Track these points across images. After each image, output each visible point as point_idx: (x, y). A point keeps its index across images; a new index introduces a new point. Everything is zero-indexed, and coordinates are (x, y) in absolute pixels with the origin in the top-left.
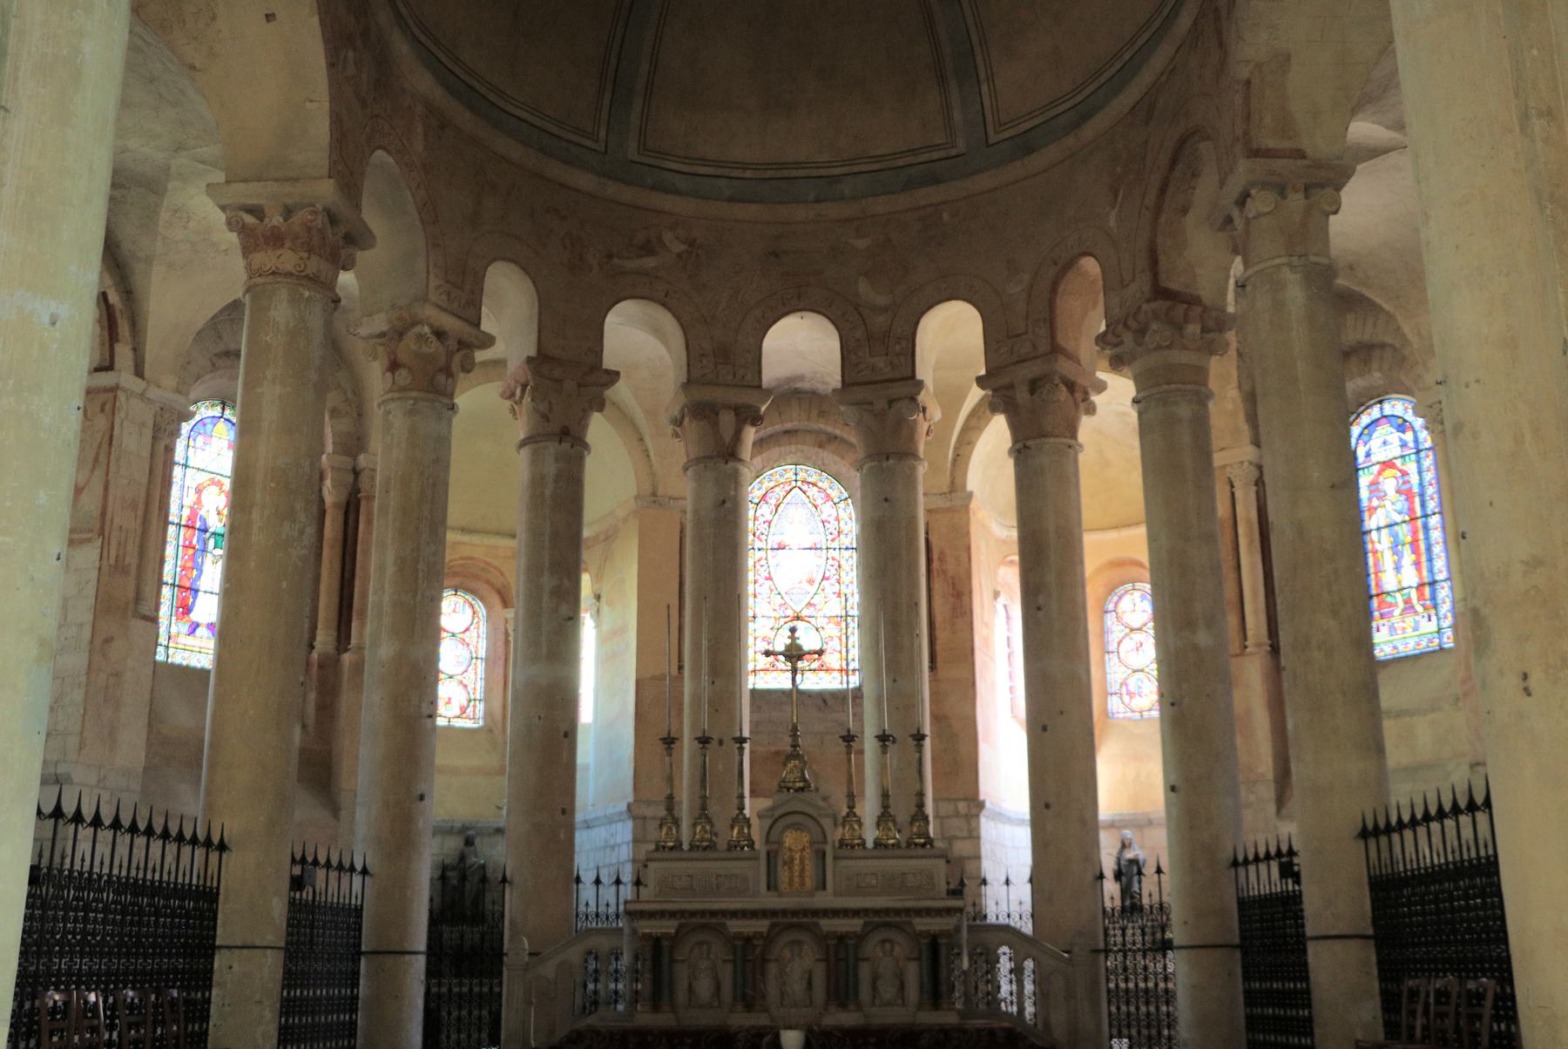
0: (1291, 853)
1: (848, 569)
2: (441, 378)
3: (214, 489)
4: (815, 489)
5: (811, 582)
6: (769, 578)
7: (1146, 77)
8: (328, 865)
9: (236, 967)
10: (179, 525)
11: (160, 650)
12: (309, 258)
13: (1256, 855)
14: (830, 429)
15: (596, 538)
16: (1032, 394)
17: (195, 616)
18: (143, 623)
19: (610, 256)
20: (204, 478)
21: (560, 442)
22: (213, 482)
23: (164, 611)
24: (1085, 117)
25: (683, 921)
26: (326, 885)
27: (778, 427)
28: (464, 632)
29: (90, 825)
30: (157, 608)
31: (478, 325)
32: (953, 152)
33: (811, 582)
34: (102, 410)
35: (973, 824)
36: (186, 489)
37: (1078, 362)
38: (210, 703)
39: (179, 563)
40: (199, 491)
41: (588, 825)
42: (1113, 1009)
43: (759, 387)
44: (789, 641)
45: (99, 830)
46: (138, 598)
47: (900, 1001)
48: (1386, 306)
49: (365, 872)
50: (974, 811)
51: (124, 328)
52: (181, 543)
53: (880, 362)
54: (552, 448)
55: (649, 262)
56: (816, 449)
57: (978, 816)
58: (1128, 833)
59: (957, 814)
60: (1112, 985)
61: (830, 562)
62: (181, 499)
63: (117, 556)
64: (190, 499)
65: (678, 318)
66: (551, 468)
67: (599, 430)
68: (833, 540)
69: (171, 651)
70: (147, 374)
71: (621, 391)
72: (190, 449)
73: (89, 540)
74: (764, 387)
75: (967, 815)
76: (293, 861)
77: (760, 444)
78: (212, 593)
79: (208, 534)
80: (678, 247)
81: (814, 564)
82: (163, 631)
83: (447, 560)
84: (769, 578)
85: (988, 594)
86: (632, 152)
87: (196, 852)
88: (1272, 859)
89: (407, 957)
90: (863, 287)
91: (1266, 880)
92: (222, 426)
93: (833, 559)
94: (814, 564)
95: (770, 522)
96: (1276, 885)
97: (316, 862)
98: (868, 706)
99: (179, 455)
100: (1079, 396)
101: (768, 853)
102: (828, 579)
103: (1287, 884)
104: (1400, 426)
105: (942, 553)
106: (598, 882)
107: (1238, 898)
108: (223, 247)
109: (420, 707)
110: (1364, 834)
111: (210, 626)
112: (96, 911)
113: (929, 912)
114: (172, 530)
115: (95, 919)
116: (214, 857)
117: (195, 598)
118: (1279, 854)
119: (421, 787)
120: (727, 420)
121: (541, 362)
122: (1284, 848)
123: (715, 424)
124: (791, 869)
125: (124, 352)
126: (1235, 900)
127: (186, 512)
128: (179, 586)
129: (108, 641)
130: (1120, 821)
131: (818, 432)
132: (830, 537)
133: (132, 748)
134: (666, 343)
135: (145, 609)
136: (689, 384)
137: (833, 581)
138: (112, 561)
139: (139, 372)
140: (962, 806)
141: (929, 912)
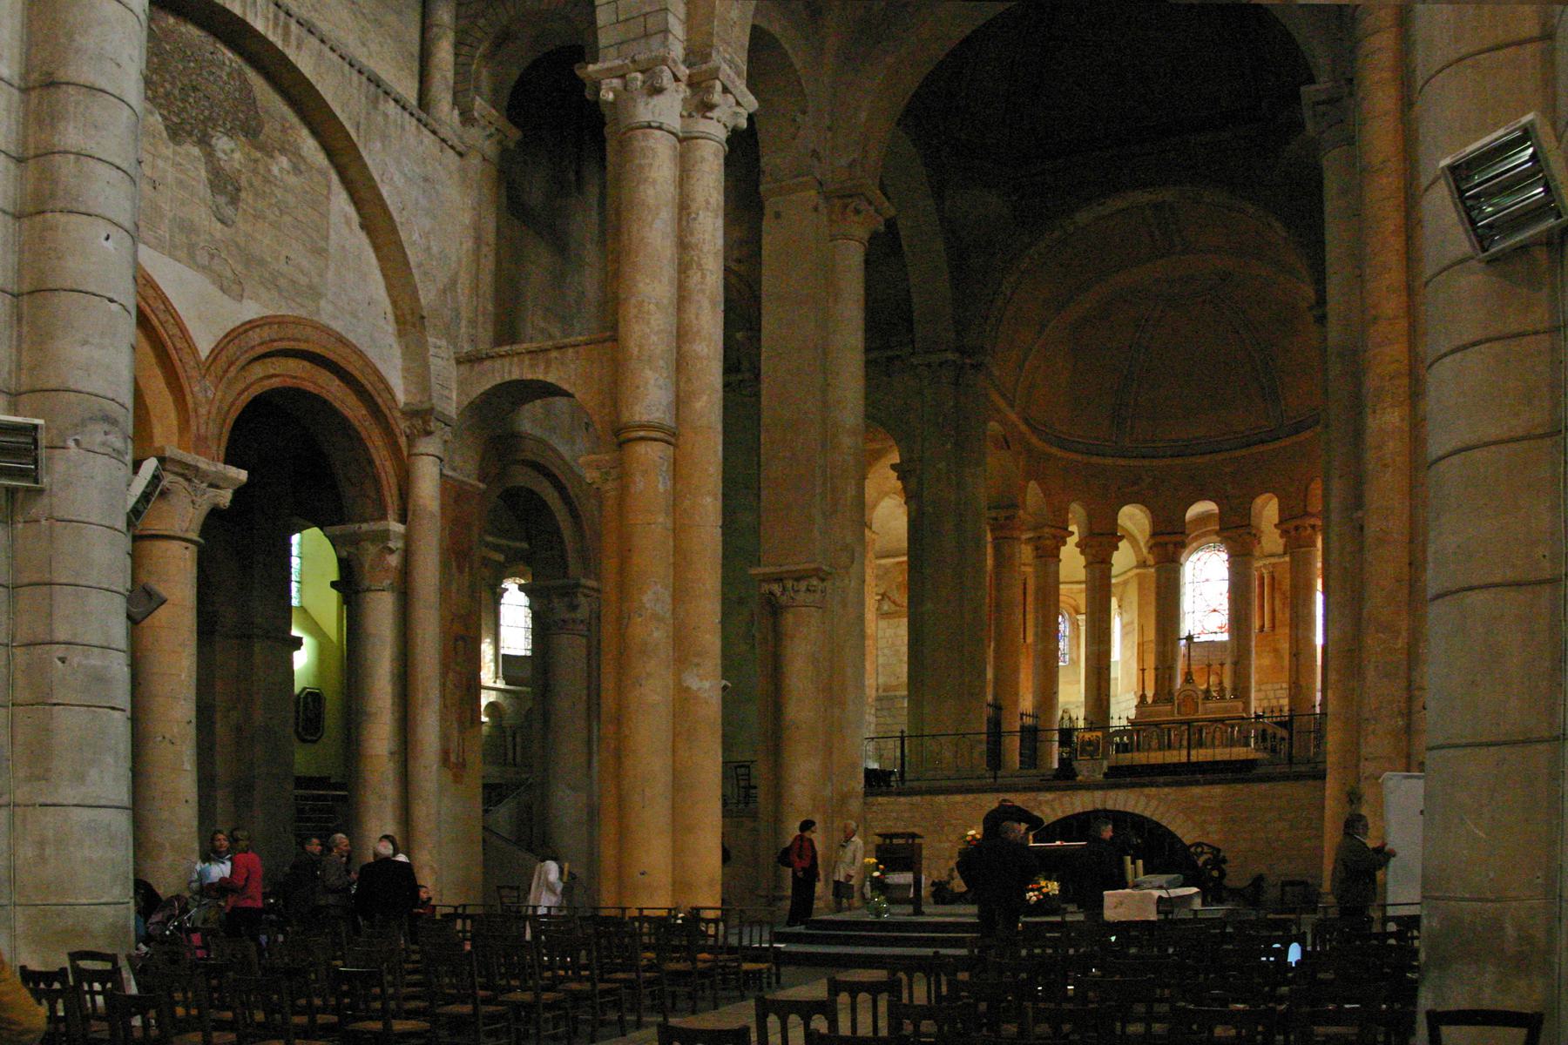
2: (1055, 551)
120: (1171, 547)
136: (1154, 534)
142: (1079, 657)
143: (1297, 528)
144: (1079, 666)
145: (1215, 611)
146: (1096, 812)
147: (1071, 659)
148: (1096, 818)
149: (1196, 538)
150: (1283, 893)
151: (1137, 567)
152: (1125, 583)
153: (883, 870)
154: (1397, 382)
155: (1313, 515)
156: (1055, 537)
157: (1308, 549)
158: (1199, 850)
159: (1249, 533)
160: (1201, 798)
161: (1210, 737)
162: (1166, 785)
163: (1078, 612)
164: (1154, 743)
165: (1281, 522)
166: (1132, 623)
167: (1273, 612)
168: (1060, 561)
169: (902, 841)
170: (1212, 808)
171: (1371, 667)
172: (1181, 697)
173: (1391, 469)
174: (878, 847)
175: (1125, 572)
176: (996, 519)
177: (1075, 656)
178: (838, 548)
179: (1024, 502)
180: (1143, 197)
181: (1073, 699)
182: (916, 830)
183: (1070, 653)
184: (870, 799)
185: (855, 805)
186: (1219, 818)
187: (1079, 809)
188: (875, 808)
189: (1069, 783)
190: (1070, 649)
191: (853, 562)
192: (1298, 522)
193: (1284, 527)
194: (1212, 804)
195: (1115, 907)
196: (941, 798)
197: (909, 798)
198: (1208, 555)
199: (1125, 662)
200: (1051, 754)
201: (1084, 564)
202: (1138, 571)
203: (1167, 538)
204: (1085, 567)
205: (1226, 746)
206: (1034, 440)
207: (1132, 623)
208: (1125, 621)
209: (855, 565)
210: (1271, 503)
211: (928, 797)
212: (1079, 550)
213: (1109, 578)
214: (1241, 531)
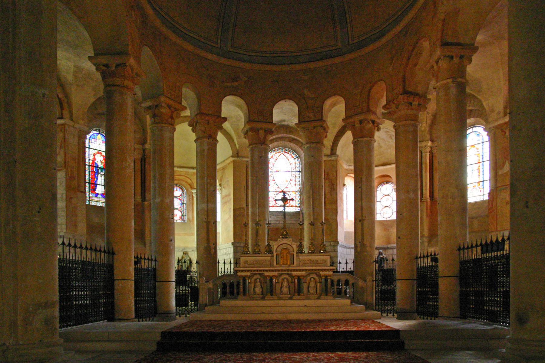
0: (435, 255)
1: (298, 178)
3: (99, 155)
4: (288, 154)
5: (287, 181)
6: (274, 180)
7: (405, 21)
8: (145, 259)
9: (121, 285)
10: (89, 165)
11: (87, 201)
12: (125, 81)
13: (464, 247)
14: (293, 136)
15: (220, 169)
16: (360, 124)
17: (97, 191)
18: (81, 194)
20: (95, 152)
21: (209, 139)
22: (98, 153)
23: (87, 190)
24: (383, 35)
25: (252, 273)
26: (145, 264)
27: (276, 136)
28: (180, 196)
29: (73, 247)
30: (85, 189)
31: (181, 103)
33: (287, 181)
34: (61, 131)
36: (90, 155)
37: (376, 114)
39: (90, 176)
40: (94, 155)
42: (377, 295)
43: (272, 122)
44: (283, 196)
45: (76, 249)
46: (79, 186)
47: (316, 293)
48: (479, 97)
49: (155, 260)
50: (336, 244)
51: (65, 105)
52: (90, 171)
53: (311, 115)
54: (206, 140)
56: (289, 143)
58: (381, 251)
60: (377, 290)
61: (293, 175)
62: (89, 158)
63: (71, 174)
64: (92, 158)
66: (206, 147)
67: (220, 136)
68: (294, 169)
69: (90, 202)
70: (74, 119)
71: (226, 125)
72: (90, 143)
73: (62, 170)
74: (274, 122)
75: (333, 246)
76: (135, 257)
77: (272, 141)
78: (101, 185)
79: (98, 168)
82: (87, 196)
83: (269, 175)
84: (274, 180)
85: (342, 185)
87: (106, 255)
88: (469, 248)
89: (170, 283)
90: (306, 91)
91: (428, 262)
92: (99, 136)
93: (294, 175)
94: (288, 176)
95: (274, 164)
96: (429, 263)
97: (141, 258)
98: (306, 216)
99: (87, 145)
100: (376, 125)
101: (276, 255)
102: (292, 180)
103: (433, 263)
104: (478, 135)
106: (224, 263)
107: (417, 267)
108: (95, 80)
109: (169, 216)
110: (459, 249)
111: (102, 195)
112: (78, 270)
113: (325, 270)
114: (87, 167)
115: (78, 272)
116: (111, 256)
117: (96, 186)
118: (431, 255)
119: (171, 238)
120: (262, 133)
121: (200, 113)
122: (433, 254)
123: (258, 134)
124: (284, 259)
125: (66, 113)
126: (416, 267)
127: (91, 162)
128: (91, 183)
129: (71, 198)
130: (379, 247)
131: (289, 138)
132: (293, 168)
133: (82, 228)
135: (82, 189)
136: (249, 121)
137: (294, 181)
138: (69, 176)
139: (71, 119)
141: (325, 270)
142: (193, 217)
144: (193, 224)
147: (188, 219)
151: (232, 156)
152: (224, 169)
156: (169, 107)
157: (369, 139)
163: (192, 188)
166: (229, 195)
172: (279, 249)
175: (224, 161)
176: (106, 66)
177: (191, 217)
181: (190, 246)
183: (188, 215)
190: (188, 212)
198: (277, 155)
199: (225, 222)
200: (168, 293)
202: (233, 159)
203: (259, 125)
207: (229, 195)
208: (224, 194)
214: (315, 124)
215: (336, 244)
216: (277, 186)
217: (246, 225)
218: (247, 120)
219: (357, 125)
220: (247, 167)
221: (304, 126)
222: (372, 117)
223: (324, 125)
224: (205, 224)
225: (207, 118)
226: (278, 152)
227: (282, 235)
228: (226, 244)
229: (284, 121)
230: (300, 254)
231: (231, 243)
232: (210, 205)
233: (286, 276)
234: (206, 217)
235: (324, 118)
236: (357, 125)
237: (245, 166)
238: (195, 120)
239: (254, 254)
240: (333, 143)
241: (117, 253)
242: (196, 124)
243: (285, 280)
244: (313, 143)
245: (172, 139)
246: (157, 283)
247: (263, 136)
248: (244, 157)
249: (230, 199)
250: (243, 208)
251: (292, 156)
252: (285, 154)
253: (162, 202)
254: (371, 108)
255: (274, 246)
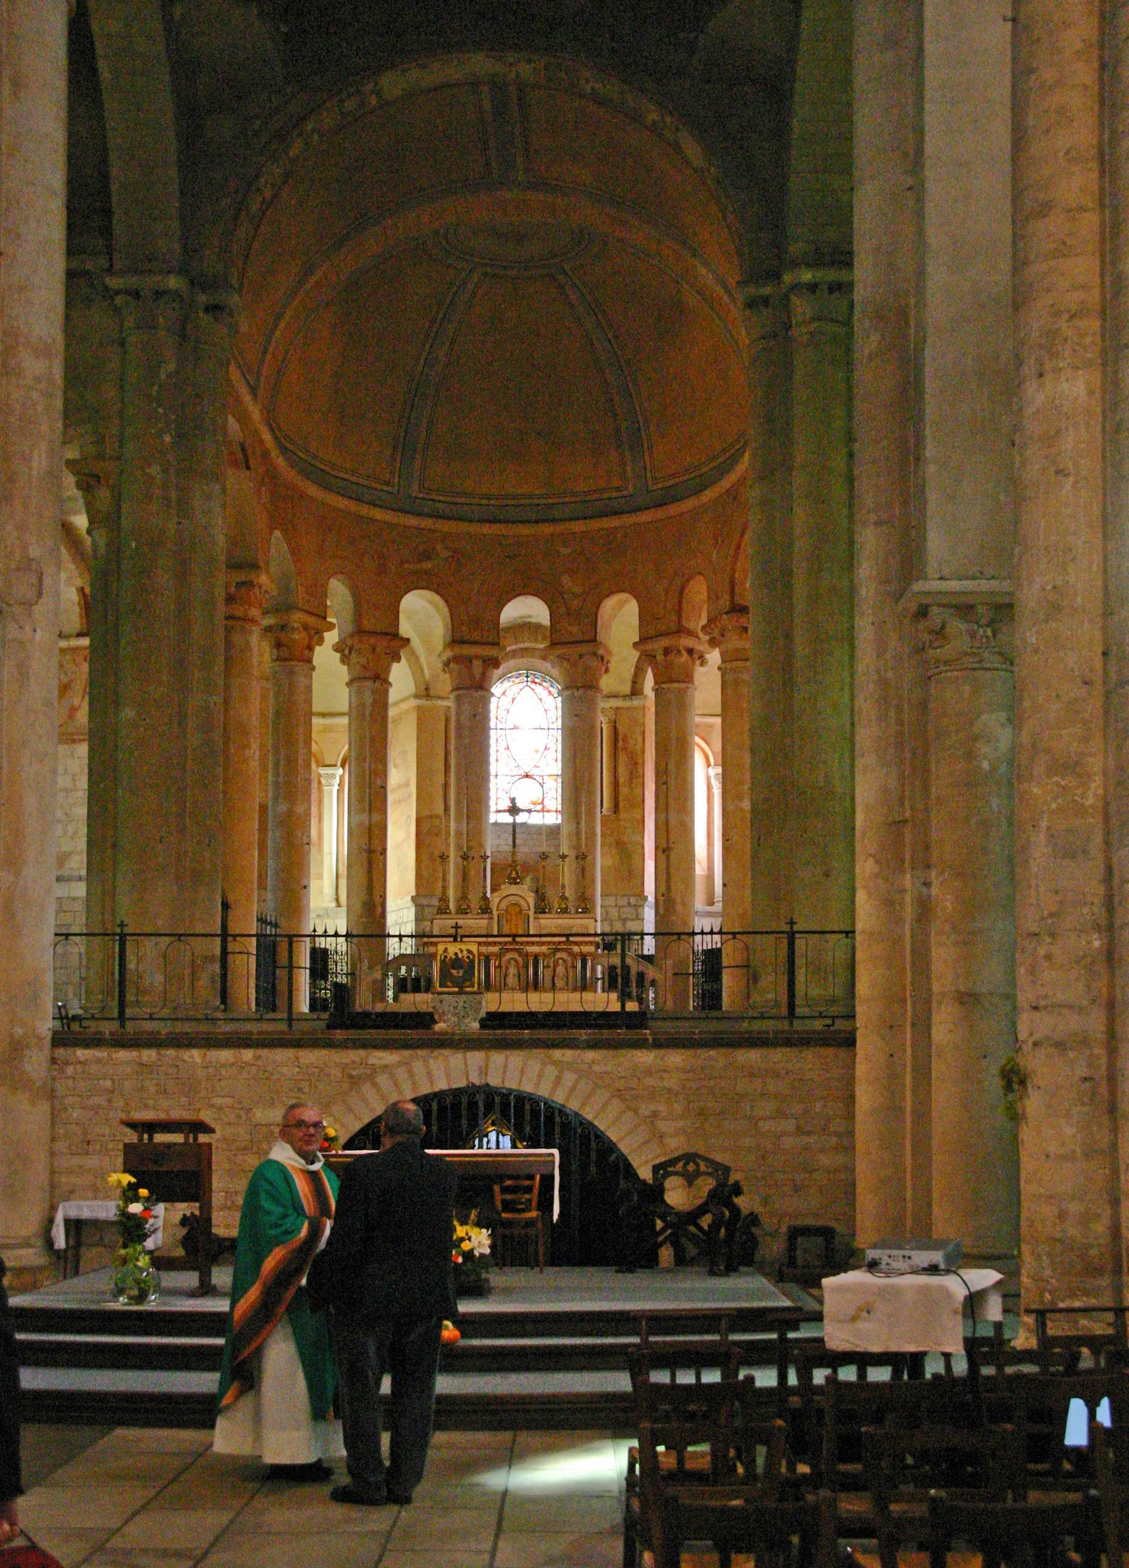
2: (306, 652)
5: (537, 751)
6: (508, 748)
19: (402, 562)
32: (625, 493)
33: (537, 751)
35: (640, 910)
38: (681, 1338)
41: (394, 790)
50: (640, 902)
53: (575, 630)
54: (368, 684)
55: (428, 565)
57: (643, 906)
59: (629, 904)
65: (446, 601)
66: (368, 699)
80: (447, 554)
81: (541, 739)
86: (415, 491)
90: (566, 580)
94: (541, 739)
100: (695, 656)
105: (625, 736)
119: (304, 883)
120: (477, 665)
123: (470, 668)
134: (438, 610)
136: (455, 641)
140: (633, 900)
143: (667, 651)
145: (527, 776)
146: (471, 1091)
148: (489, 1107)
149: (514, 654)
150: (792, 1248)
151: (416, 696)
153: (148, 1199)
154: (1083, 324)
155: (690, 633)
156: (306, 627)
157: (682, 685)
158: (691, 1167)
159: (595, 654)
160: (649, 1073)
161: (548, 973)
162: (592, 1045)
164: (512, 980)
165: (643, 640)
166: (407, 785)
167: (615, 785)
168: (313, 669)
169: (178, 1138)
170: (669, 1090)
171: (1041, 839)
172: (504, 905)
173: (1071, 479)
174: (128, 1148)
178: (13, 565)
179: (267, 563)
180: (481, 64)
182: (206, 1116)
184: (61, 1052)
185: (36, 1063)
186: (678, 1108)
187: (442, 1085)
188: (70, 1070)
189: (714, 1014)
191: (40, 595)
192: (665, 642)
193: (649, 646)
194: (666, 1084)
195: (854, 1319)
196: (196, 1055)
197: (135, 1053)
198: (516, 688)
201: (347, 679)
204: (348, 684)
205: (575, 990)
206: (281, 462)
207: (407, 785)
209: (44, 599)
210: (627, 607)
211: (171, 1052)
212: (338, 655)
213: (385, 706)
214: (583, 649)
215: (640, 902)
216: (514, 764)
217: (444, 858)
218: (449, 639)
219: (660, 657)
220: (447, 720)
221: (559, 652)
222: (689, 642)
223: (601, 652)
224: (365, 855)
225: (372, 640)
226: (517, 680)
227: (509, 877)
228: (399, 901)
229: (530, 616)
230: (541, 916)
231: (409, 898)
232: (376, 817)
233: (516, 956)
234: (366, 841)
235: (600, 637)
236: (660, 657)
237: (443, 718)
238: (349, 642)
239: (457, 913)
240: (636, 667)
241: (233, 906)
242: (350, 651)
243: (513, 962)
244: (578, 688)
245: (309, 688)
246: (278, 971)
247: (481, 670)
248: (440, 698)
249: (410, 796)
250: (437, 817)
251: (550, 692)
252: (533, 686)
253: (290, 813)
254: (685, 623)
255: (494, 900)
